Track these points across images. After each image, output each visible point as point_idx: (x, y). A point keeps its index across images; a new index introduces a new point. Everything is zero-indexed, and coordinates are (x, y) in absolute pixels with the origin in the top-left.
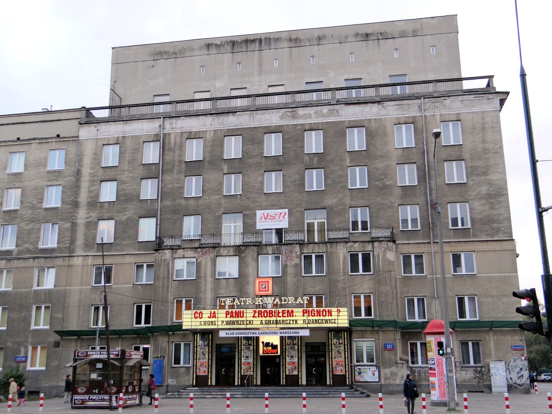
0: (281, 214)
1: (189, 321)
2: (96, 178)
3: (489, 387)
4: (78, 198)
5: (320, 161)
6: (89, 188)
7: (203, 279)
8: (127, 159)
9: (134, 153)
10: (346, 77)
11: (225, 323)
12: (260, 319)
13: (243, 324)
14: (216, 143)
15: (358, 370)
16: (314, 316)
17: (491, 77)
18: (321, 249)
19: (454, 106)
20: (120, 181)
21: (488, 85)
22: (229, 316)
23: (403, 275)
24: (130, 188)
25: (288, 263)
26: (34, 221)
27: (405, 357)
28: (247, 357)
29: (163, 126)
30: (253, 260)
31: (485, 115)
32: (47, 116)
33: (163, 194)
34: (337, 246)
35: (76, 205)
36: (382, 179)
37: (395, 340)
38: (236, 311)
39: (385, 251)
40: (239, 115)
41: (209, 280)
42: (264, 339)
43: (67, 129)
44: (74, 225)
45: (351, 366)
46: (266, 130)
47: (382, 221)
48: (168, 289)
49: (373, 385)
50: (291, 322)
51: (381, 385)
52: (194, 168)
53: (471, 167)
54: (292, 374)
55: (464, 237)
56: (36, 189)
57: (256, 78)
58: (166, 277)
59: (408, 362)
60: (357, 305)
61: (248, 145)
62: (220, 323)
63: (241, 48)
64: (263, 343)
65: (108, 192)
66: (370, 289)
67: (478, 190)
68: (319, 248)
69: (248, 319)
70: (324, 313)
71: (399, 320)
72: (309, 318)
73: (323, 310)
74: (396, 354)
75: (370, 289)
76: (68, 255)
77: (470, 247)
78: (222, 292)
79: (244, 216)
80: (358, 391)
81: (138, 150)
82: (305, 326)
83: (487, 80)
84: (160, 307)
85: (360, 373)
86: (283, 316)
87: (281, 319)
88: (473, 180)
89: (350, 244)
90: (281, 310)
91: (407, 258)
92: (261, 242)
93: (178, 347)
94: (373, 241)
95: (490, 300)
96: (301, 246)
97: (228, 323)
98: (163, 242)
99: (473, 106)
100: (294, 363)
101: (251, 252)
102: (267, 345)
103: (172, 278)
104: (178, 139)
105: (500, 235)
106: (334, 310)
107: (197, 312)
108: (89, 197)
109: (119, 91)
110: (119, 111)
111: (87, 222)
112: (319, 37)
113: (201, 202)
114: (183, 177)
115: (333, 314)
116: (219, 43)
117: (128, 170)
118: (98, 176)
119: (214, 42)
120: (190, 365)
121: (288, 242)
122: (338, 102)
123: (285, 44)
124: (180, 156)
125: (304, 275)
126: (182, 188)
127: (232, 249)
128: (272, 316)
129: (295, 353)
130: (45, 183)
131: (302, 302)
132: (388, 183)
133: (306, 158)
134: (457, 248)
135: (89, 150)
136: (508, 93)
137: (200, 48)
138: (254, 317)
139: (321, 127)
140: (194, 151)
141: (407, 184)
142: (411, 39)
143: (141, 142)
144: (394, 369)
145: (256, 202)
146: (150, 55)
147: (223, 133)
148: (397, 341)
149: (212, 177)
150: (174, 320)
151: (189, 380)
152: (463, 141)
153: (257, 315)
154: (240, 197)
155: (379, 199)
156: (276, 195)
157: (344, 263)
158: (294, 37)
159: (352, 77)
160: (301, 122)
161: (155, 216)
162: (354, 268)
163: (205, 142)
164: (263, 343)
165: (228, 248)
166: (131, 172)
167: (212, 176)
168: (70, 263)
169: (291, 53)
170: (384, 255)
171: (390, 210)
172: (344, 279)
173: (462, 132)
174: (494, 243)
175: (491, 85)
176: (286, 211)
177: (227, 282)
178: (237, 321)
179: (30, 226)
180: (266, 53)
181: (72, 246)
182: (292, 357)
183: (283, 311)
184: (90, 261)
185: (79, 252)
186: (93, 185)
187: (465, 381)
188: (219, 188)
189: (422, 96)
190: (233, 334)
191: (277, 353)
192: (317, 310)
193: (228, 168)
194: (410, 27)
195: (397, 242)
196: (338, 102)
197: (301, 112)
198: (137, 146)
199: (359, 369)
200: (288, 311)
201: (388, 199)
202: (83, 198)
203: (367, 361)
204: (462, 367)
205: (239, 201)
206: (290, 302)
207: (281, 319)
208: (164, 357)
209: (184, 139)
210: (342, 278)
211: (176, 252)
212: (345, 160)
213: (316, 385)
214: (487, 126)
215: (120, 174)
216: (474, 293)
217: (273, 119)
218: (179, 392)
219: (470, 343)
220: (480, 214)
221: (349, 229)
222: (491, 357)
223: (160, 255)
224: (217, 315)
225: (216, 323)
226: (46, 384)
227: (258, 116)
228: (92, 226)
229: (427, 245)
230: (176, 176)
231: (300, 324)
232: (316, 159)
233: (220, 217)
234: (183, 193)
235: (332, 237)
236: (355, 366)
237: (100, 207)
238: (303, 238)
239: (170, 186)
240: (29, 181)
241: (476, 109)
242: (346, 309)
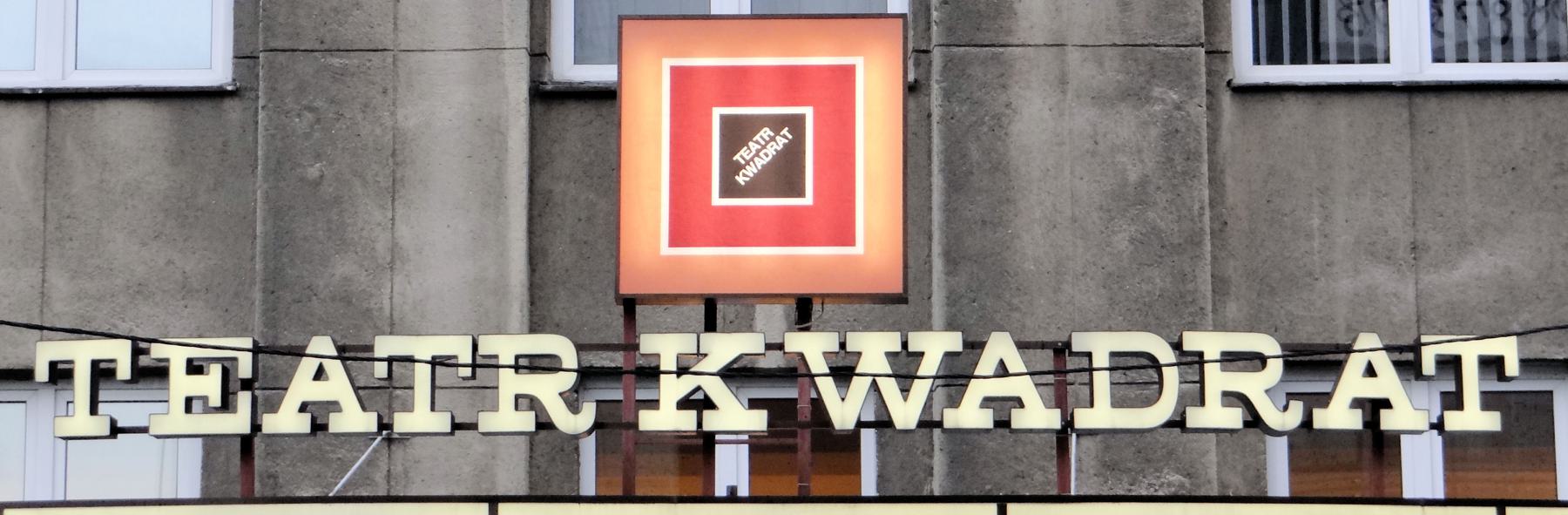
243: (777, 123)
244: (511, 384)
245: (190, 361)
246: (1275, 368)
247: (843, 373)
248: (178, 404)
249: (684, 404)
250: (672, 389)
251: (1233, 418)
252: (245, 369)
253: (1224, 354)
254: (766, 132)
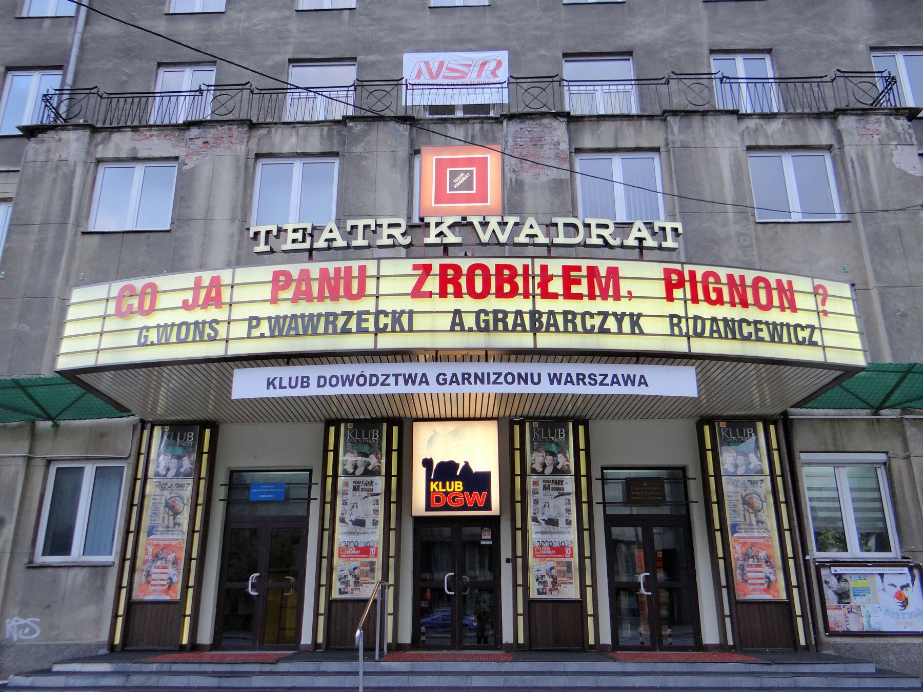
0: (484, 64)
1: (93, 330)
11: (264, 328)
12: (451, 303)
13: (361, 331)
15: (833, 581)
16: (720, 301)
22: (288, 294)
25: (527, 177)
28: (360, 523)
30: (394, 165)
34: (704, 127)
38: (324, 272)
42: (434, 443)
49: (907, 649)
50: (611, 324)
54: (555, 596)
58: (55, 217)
62: (239, 330)
64: (427, 463)
68: (638, 132)
69: (387, 305)
70: (763, 294)
72: (694, 310)
73: (757, 280)
82: (679, 345)
84: (14, 325)
85: (843, 596)
86: (568, 295)
87: (561, 305)
90: (555, 267)
93: (67, 482)
96: (573, 126)
97: (279, 327)
100: (560, 550)
102: (445, 471)
103: (77, 225)
106: (801, 284)
107: (131, 288)
113: (221, 26)
115: (800, 301)
127: (315, 132)
128: (513, 293)
129: (565, 507)
138: (417, 293)
151: (98, 621)
153: (432, 284)
154: (351, 17)
155: (802, 31)
156: (467, 12)
164: (427, 463)
165: (302, 130)
172: (739, 234)
176: (503, 55)
178: (331, 317)
182: (552, 522)
183: (567, 270)
191: (488, 506)
192: (730, 277)
199: (839, 577)
200: (592, 272)
203: (864, 546)
207: (561, 305)
210: (733, 229)
213: (656, 643)
223: (44, 147)
224: (226, 296)
225: (222, 330)
231: (655, 336)
243: (465, 172)
244: (386, 231)
245: (364, 526)
246: (612, 228)
247: (485, 224)
248: (289, 241)
249: (438, 236)
250: (434, 231)
251: (600, 242)
252: (309, 231)
253: (582, 299)
254: (462, 174)
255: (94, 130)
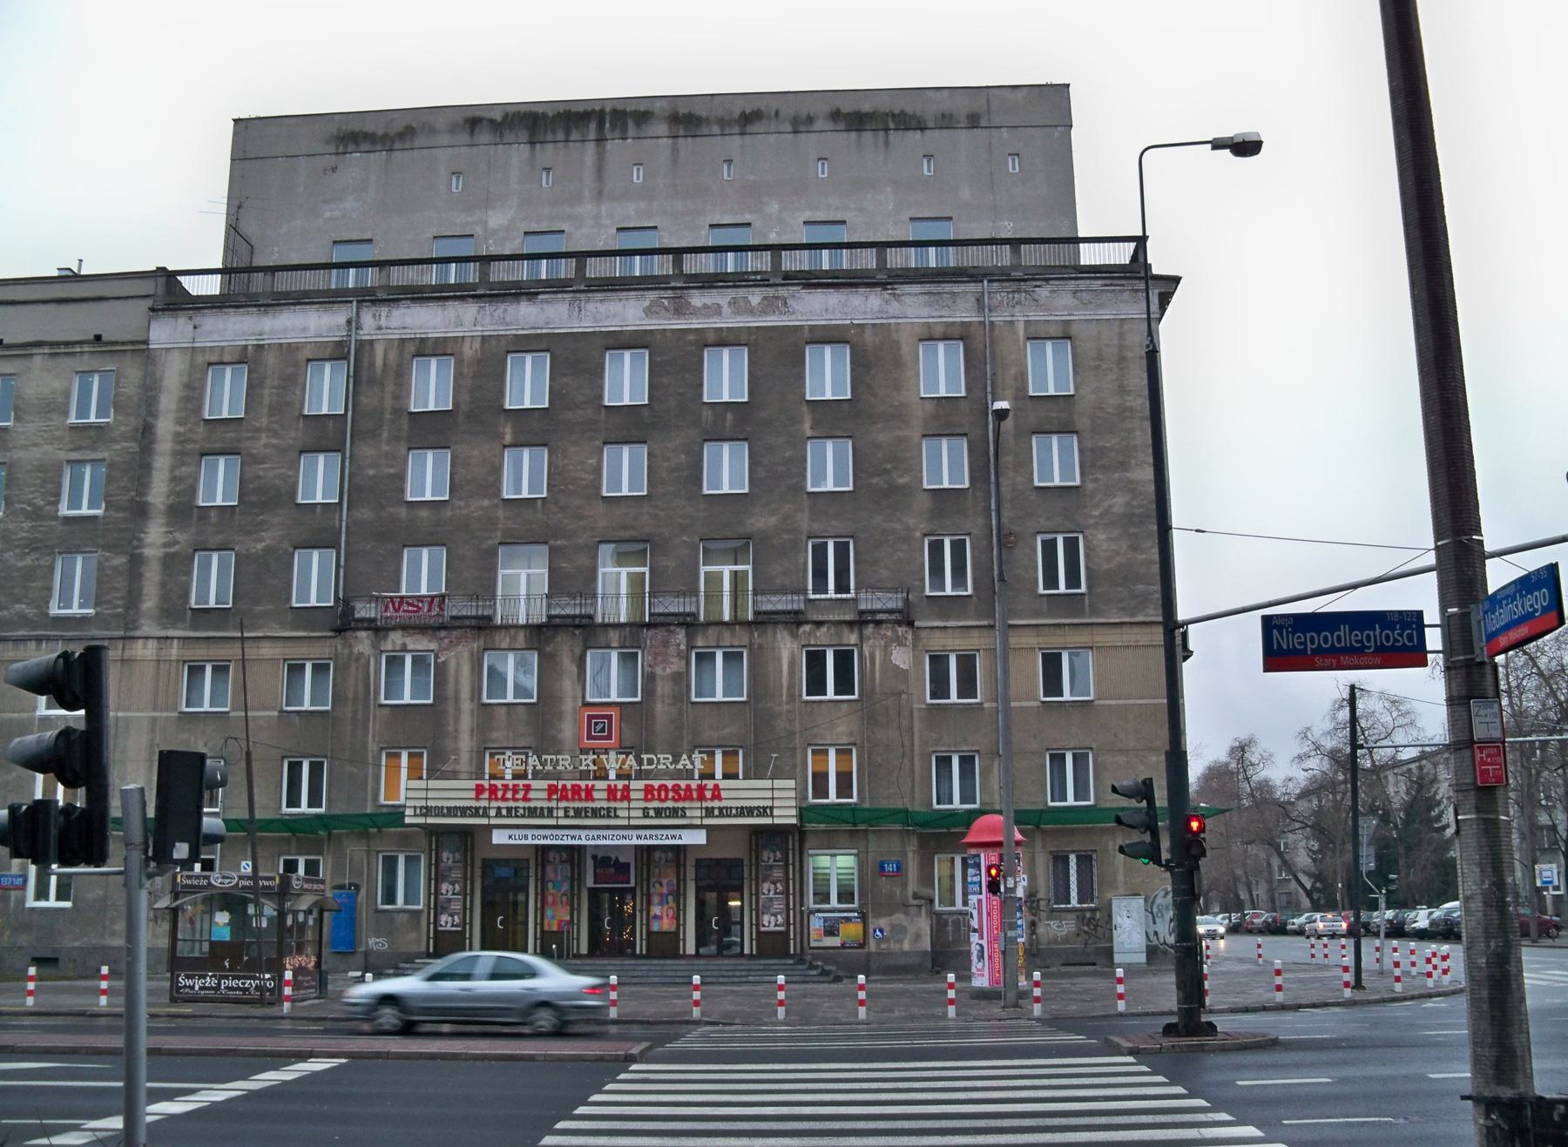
2: (189, 447)
3: (1109, 953)
4: (145, 495)
5: (735, 422)
6: (172, 471)
7: (451, 703)
8: (266, 401)
9: (284, 388)
10: (808, 215)
14: (483, 370)
17: (1141, 241)
18: (742, 637)
19: (1056, 302)
20: (249, 454)
21: (1135, 258)
23: (929, 701)
24: (270, 474)
25: (658, 671)
26: (36, 549)
27: (926, 891)
29: (358, 322)
31: (1126, 327)
32: (70, 289)
33: (355, 489)
34: (775, 634)
35: (140, 511)
36: (886, 471)
37: (904, 853)
39: (886, 646)
40: (542, 302)
41: (466, 706)
43: (118, 321)
44: (136, 561)
45: (802, 912)
46: (611, 341)
47: (884, 573)
48: (366, 727)
51: (869, 954)
52: (430, 430)
53: (1092, 450)
55: (1070, 616)
56: (41, 468)
57: (587, 208)
59: (931, 901)
60: (818, 769)
61: (564, 375)
63: (554, 131)
65: (219, 486)
66: (851, 734)
67: (1105, 504)
68: (733, 635)
71: (918, 807)
74: (905, 885)
75: (851, 734)
76: (121, 633)
77: (1083, 638)
78: (498, 736)
79: (552, 551)
80: (816, 967)
81: (292, 380)
83: (1133, 245)
88: (1096, 480)
89: (807, 628)
91: (939, 662)
92: (591, 617)
93: (390, 864)
94: (862, 621)
95: (1121, 759)
98: (353, 609)
99: (1101, 306)
101: (565, 647)
104: (392, 356)
105: (1151, 612)
108: (172, 493)
109: (249, 228)
110: (249, 279)
111: (167, 555)
112: (748, 115)
114: (404, 451)
116: (499, 118)
117: (268, 429)
118: (194, 441)
119: (487, 115)
120: (420, 907)
121: (662, 619)
122: (790, 278)
123: (662, 129)
124: (396, 398)
125: (694, 699)
126: (401, 477)
130: (63, 455)
131: (689, 767)
132: (901, 481)
133: (707, 414)
134: (1053, 641)
135: (172, 375)
136: (1176, 280)
137: (453, 129)
139: (743, 340)
140: (432, 389)
141: (946, 485)
142: (963, 135)
143: (296, 361)
144: (899, 917)
145: (581, 517)
146: (328, 142)
147: (503, 343)
148: (910, 855)
149: (476, 453)
150: (382, 801)
151: (419, 940)
152: (1076, 389)
155: (878, 519)
157: (792, 673)
158: (682, 110)
159: (821, 216)
160: (696, 323)
161: (335, 545)
162: (816, 685)
163: (459, 364)
166: (275, 434)
167: (476, 451)
168: (127, 654)
169: (675, 151)
170: (887, 654)
171: (905, 547)
173: (1075, 365)
174: (1136, 629)
175: (1141, 259)
177: (509, 713)
179: (28, 561)
180: (613, 146)
181: (132, 612)
184: (174, 651)
185: (148, 628)
186: (183, 464)
187: (1055, 941)
188: (491, 479)
189: (985, 275)
190: (526, 837)
193: (515, 432)
194: (962, 107)
195: (917, 624)
196: (790, 278)
197: (698, 299)
198: (291, 370)
201: (899, 520)
202: (158, 493)
203: (839, 901)
204: (1053, 910)
205: (540, 515)
206: (661, 767)
208: (357, 888)
209: (407, 356)
210: (786, 707)
211: (385, 637)
212: (801, 422)
214: (1130, 355)
215: (248, 439)
216: (1086, 744)
217: (628, 313)
218: (397, 968)
219: (1073, 858)
220: (1108, 560)
221: (805, 591)
222: (1116, 888)
226: (75, 940)
227: (591, 307)
228: (177, 565)
229: (986, 632)
230: (385, 448)
232: (729, 416)
233: (493, 553)
234: (403, 491)
235: (769, 607)
236: (812, 912)
237: (200, 518)
238: (694, 609)
239: (371, 472)
240: (25, 447)
241: (1106, 314)
242: (791, 783)
255: (377, 630)
